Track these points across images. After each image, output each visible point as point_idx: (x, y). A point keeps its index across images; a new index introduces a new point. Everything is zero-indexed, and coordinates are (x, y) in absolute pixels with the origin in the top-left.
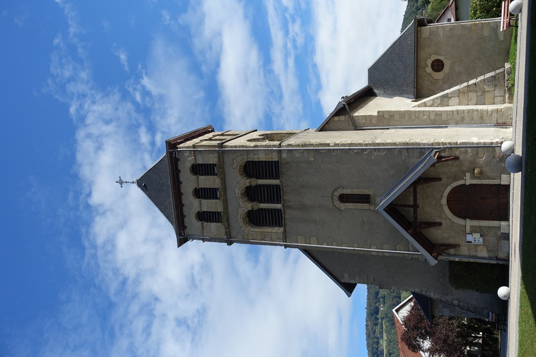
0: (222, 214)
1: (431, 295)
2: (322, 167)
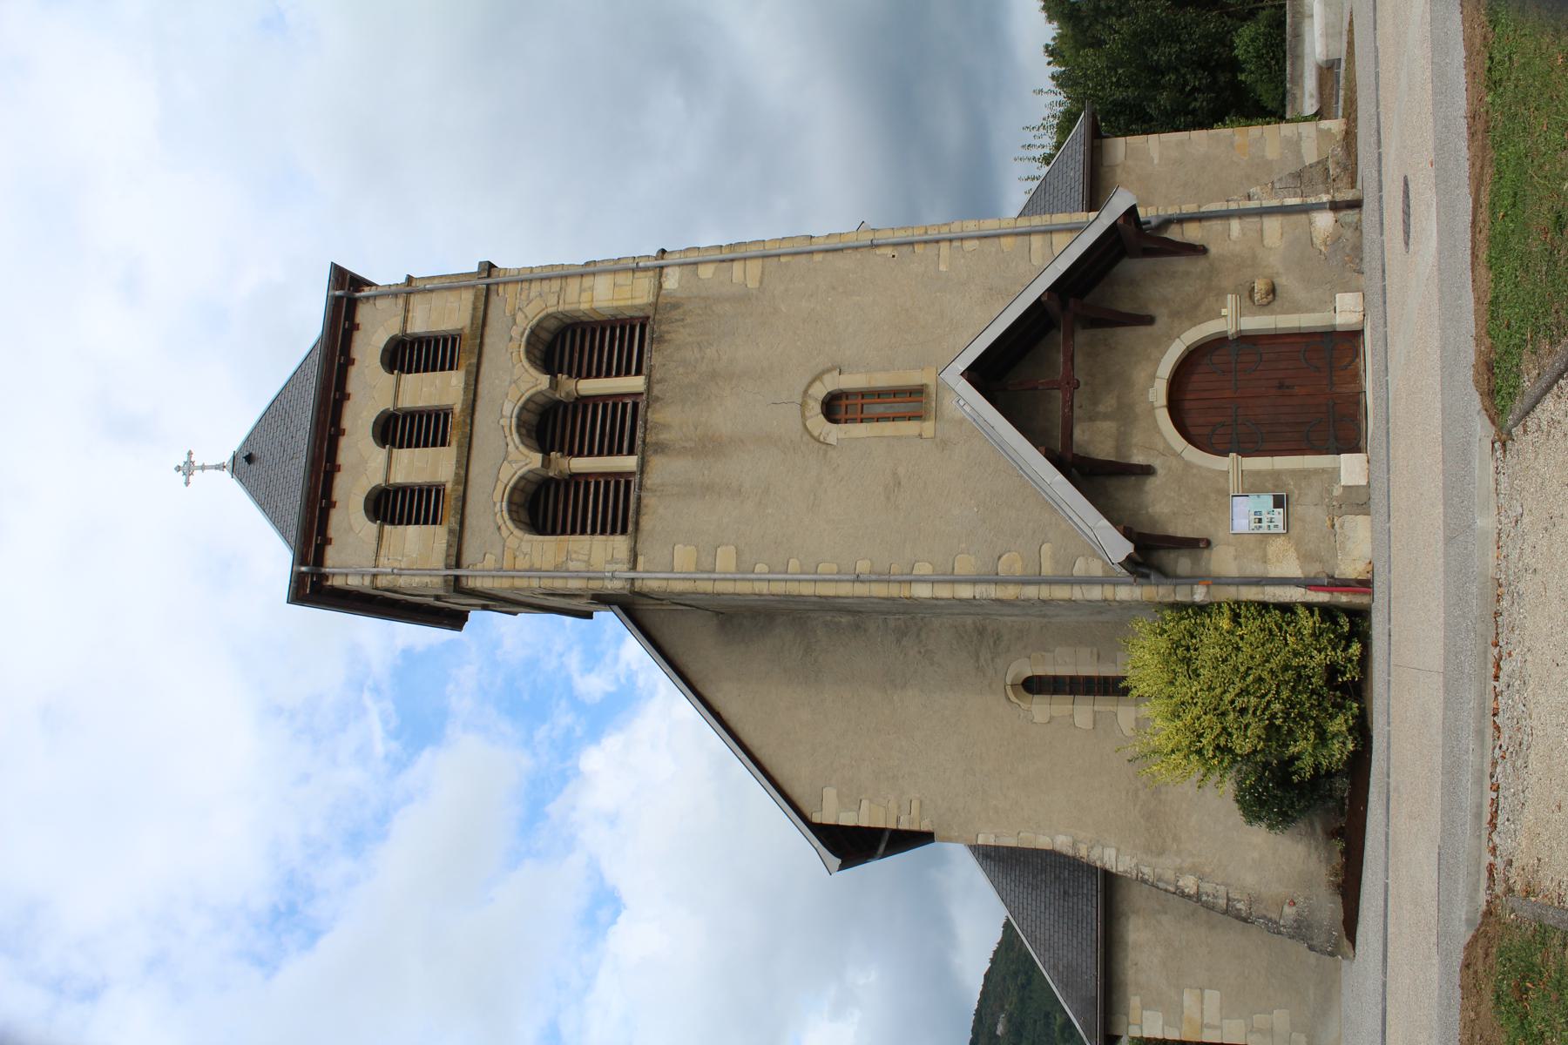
1: (1106, 858)
2: (783, 309)
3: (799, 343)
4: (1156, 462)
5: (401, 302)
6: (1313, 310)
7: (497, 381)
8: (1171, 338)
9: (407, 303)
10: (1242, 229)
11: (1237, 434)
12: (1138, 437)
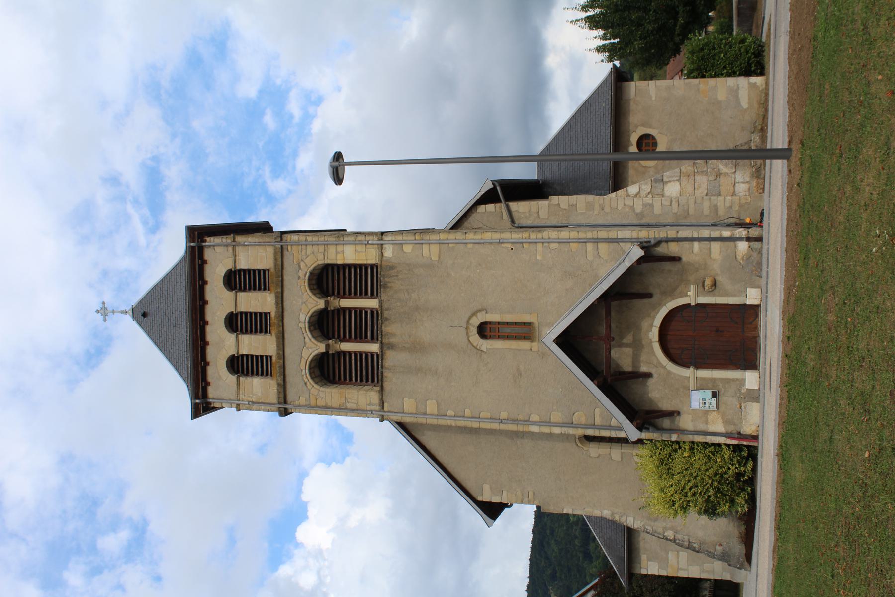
0: (274, 358)
1: (628, 522)
2: (453, 274)
3: (463, 294)
4: (653, 371)
5: (230, 249)
6: (734, 295)
7: (294, 302)
8: (660, 305)
9: (234, 251)
10: (700, 248)
12: (643, 357)
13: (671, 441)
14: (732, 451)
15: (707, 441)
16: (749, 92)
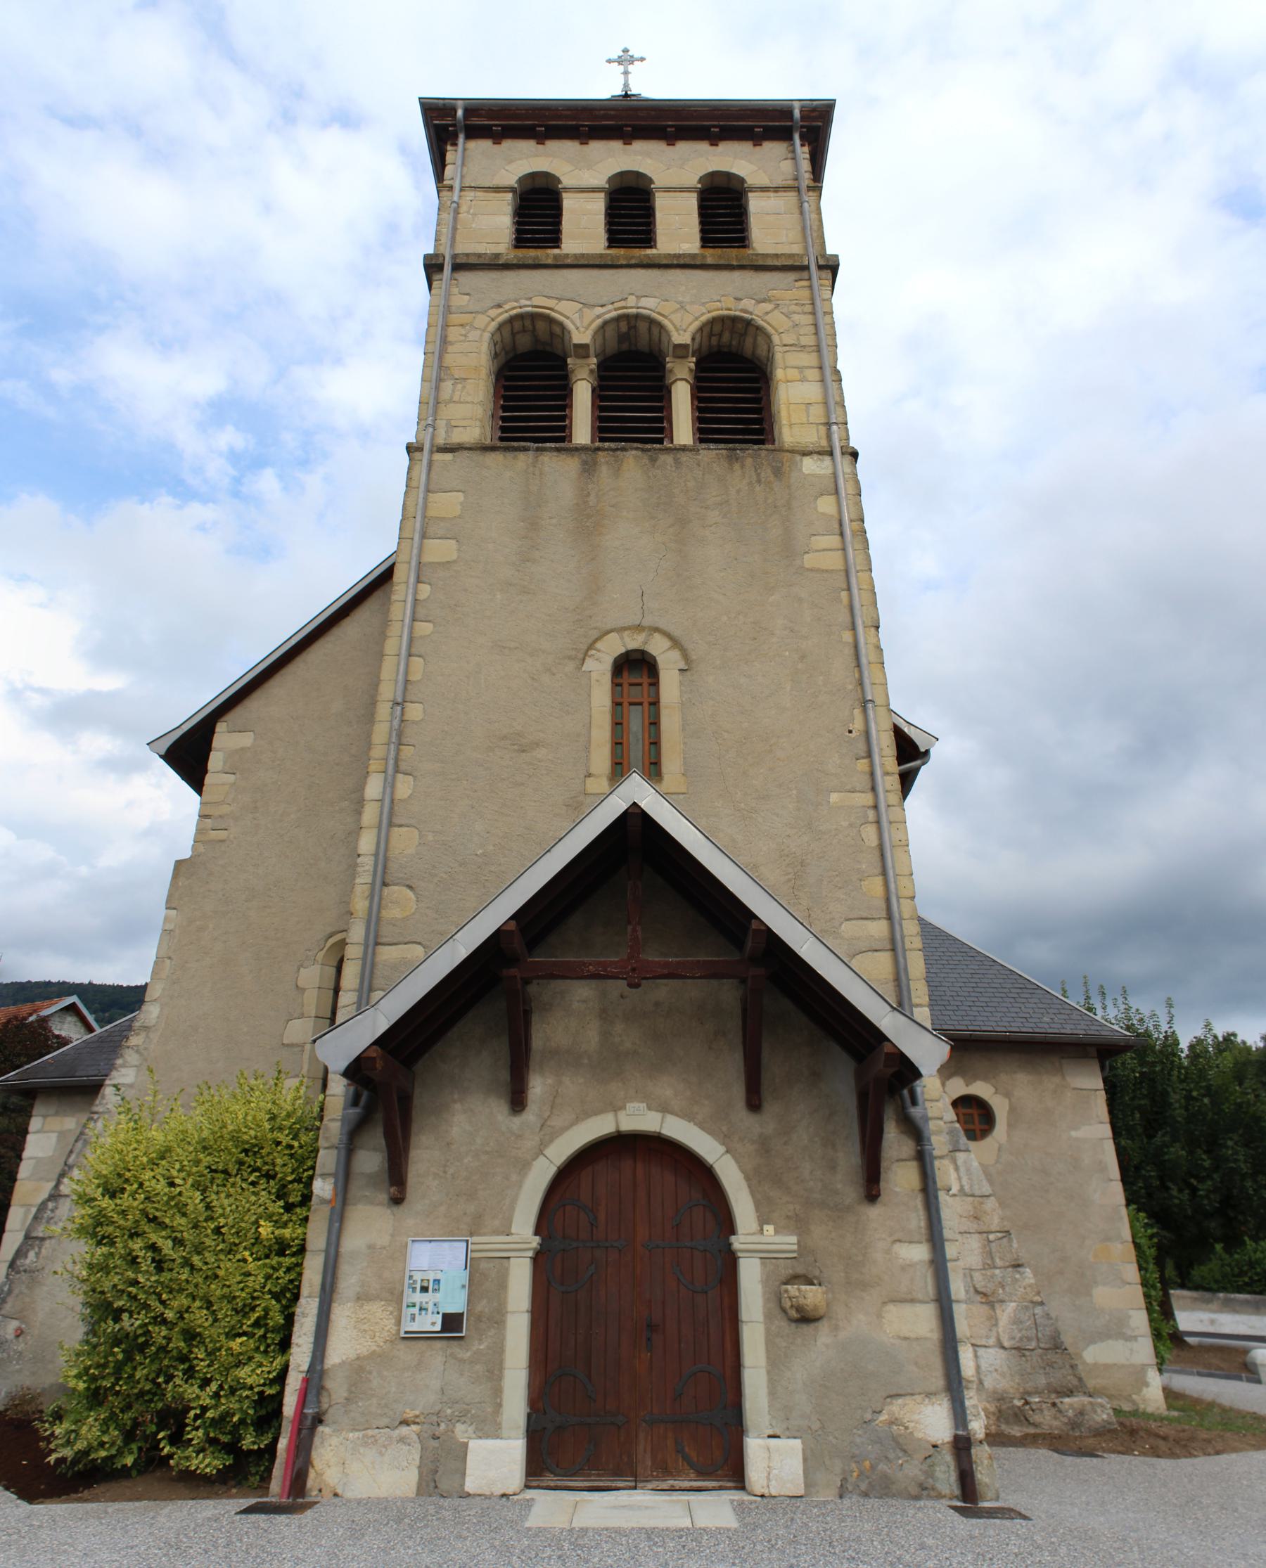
0: (556, 251)
1: (123, 1071)
4: (530, 1115)
6: (772, 1393)
8: (725, 1139)
10: (912, 1265)
11: (577, 1248)
12: (572, 1085)
13: (311, 1178)
14: (261, 1393)
15: (302, 1301)
16: (1123, 1366)
